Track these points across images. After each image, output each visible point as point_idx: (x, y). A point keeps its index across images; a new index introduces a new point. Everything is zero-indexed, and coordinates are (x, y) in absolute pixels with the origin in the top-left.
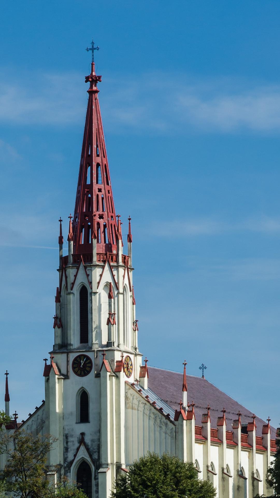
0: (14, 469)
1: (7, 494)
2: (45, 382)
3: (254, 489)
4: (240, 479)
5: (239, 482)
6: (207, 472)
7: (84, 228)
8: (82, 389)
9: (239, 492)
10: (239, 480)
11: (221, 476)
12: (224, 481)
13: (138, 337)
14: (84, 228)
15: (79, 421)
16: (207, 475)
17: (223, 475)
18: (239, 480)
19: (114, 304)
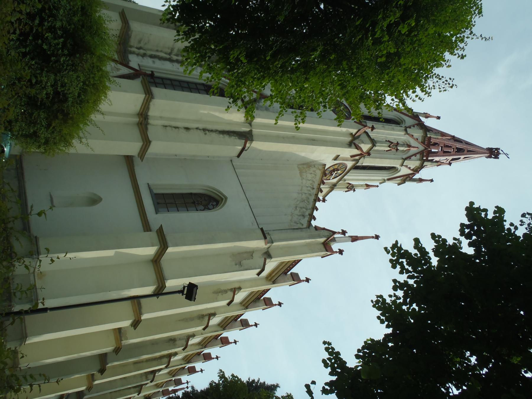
0: (60, 91)
1: (389, 141)
2: (351, 148)
3: (157, 360)
4: (184, 340)
5: (180, 339)
6: (232, 289)
7: (417, 311)
8: (223, 198)
9: (166, 342)
10: (183, 339)
11: (205, 313)
12: (200, 319)
13: (112, 389)
14: (417, 311)
15: (156, 191)
16: (228, 289)
17: (206, 315)
18: (183, 339)
19: (248, 301)
